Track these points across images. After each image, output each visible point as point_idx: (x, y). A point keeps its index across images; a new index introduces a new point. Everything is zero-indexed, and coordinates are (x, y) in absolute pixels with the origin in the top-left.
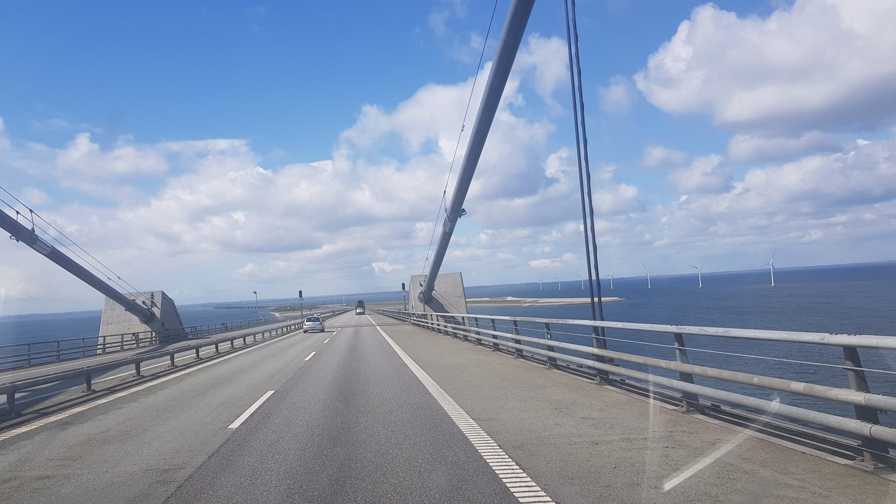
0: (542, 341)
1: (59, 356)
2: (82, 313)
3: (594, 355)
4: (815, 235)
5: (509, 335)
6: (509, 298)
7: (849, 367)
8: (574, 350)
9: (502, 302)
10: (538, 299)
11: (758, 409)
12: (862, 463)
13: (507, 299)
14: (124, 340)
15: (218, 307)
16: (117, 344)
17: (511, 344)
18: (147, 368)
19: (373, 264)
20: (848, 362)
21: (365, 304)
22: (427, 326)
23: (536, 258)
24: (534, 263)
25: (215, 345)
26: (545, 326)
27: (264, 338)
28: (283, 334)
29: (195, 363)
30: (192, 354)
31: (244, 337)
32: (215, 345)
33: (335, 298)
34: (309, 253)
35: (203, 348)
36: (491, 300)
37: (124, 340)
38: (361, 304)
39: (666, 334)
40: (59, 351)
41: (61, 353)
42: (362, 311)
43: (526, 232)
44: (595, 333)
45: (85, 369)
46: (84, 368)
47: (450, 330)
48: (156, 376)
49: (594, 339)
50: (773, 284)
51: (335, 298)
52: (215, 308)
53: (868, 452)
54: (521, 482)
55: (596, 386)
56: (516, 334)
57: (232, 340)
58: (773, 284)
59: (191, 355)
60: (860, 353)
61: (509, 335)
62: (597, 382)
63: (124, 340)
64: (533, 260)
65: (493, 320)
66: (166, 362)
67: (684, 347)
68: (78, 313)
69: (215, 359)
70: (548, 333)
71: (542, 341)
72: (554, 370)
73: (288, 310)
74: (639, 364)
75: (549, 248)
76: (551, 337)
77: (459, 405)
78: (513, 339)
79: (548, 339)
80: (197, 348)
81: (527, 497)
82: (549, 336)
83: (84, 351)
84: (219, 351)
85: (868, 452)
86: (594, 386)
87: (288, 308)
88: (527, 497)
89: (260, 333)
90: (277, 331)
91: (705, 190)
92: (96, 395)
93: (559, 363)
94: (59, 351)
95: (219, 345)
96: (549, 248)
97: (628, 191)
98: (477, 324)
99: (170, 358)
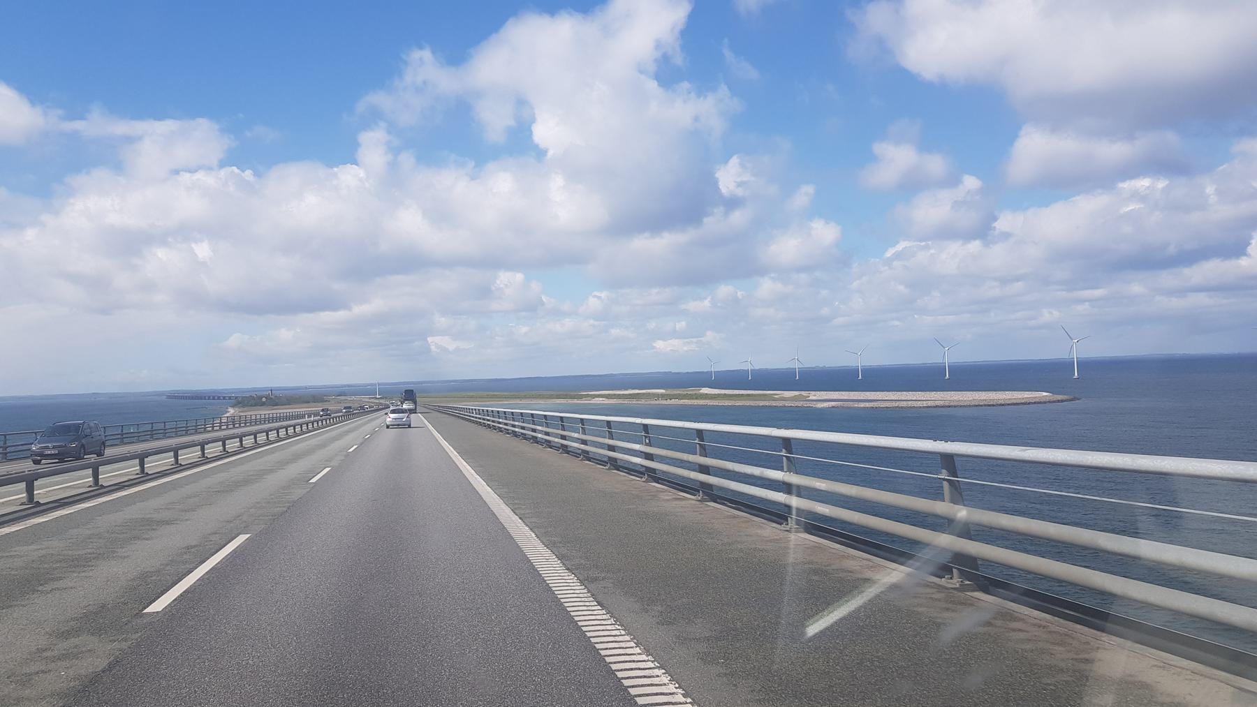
0: (691, 458)
1: (6, 454)
2: (32, 398)
3: (645, 453)
4: (1049, 315)
5: (637, 447)
6: (705, 390)
7: (943, 477)
8: (806, 487)
9: (691, 397)
10: (804, 393)
11: (915, 540)
12: (951, 581)
13: (701, 391)
14: (124, 432)
15: (175, 396)
16: (117, 437)
17: (556, 440)
18: (46, 490)
19: (428, 339)
20: (944, 471)
21: (417, 395)
22: (499, 427)
23: (664, 337)
24: (659, 344)
25: (172, 453)
26: (606, 424)
27: (268, 439)
28: (296, 435)
29: (89, 495)
30: (132, 468)
31: (241, 437)
32: (172, 453)
33: (369, 387)
34: (326, 316)
35: (150, 458)
36: (669, 392)
37: (167, 427)
38: (409, 395)
39: (975, 460)
40: (205, 425)
41: (8, 450)
42: (412, 407)
43: (655, 294)
44: (786, 449)
45: (27, 473)
46: (24, 472)
47: (540, 436)
48: (120, 486)
49: (945, 484)
50: (1076, 374)
51: (369, 387)
52: (169, 397)
53: (956, 568)
54: (626, 648)
55: (698, 503)
56: (609, 439)
57: (241, 437)
58: (1076, 374)
59: (167, 460)
60: (585, 421)
61: (637, 447)
62: (644, 479)
63: (198, 424)
64: (659, 339)
65: (609, 423)
66: (83, 479)
67: (957, 477)
68: (41, 398)
69: (222, 458)
70: (646, 437)
71: (691, 458)
72: (708, 503)
73: (263, 404)
74: (682, 461)
75: (684, 323)
76: (650, 441)
77: (599, 604)
78: (579, 439)
79: (647, 444)
80: (142, 458)
81: (649, 685)
82: (647, 441)
83: (139, 436)
84: (206, 455)
85: (956, 568)
86: (694, 502)
87: (264, 399)
88: (649, 685)
89: (283, 428)
90: (294, 429)
91: (946, 233)
92: (183, 468)
93: (619, 463)
94: (122, 435)
95: (280, 430)
96: (684, 323)
97: (825, 233)
98: (506, 417)
99: (138, 462)
